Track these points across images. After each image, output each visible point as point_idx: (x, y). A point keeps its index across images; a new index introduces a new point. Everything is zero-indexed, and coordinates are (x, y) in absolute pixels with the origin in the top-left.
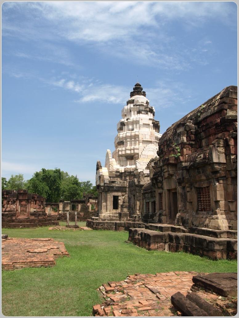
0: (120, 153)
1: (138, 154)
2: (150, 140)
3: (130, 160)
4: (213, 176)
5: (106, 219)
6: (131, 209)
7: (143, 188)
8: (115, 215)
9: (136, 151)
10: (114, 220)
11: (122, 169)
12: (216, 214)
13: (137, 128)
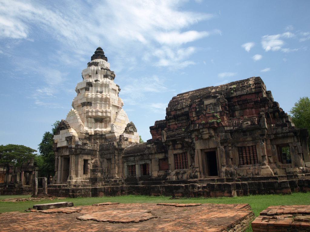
0: (90, 114)
1: (110, 117)
2: (118, 105)
3: (100, 122)
4: (261, 138)
5: (79, 186)
6: (103, 173)
7: (123, 152)
8: (86, 181)
9: (109, 115)
10: (87, 186)
11: (92, 131)
12: (264, 164)
13: (106, 91)
